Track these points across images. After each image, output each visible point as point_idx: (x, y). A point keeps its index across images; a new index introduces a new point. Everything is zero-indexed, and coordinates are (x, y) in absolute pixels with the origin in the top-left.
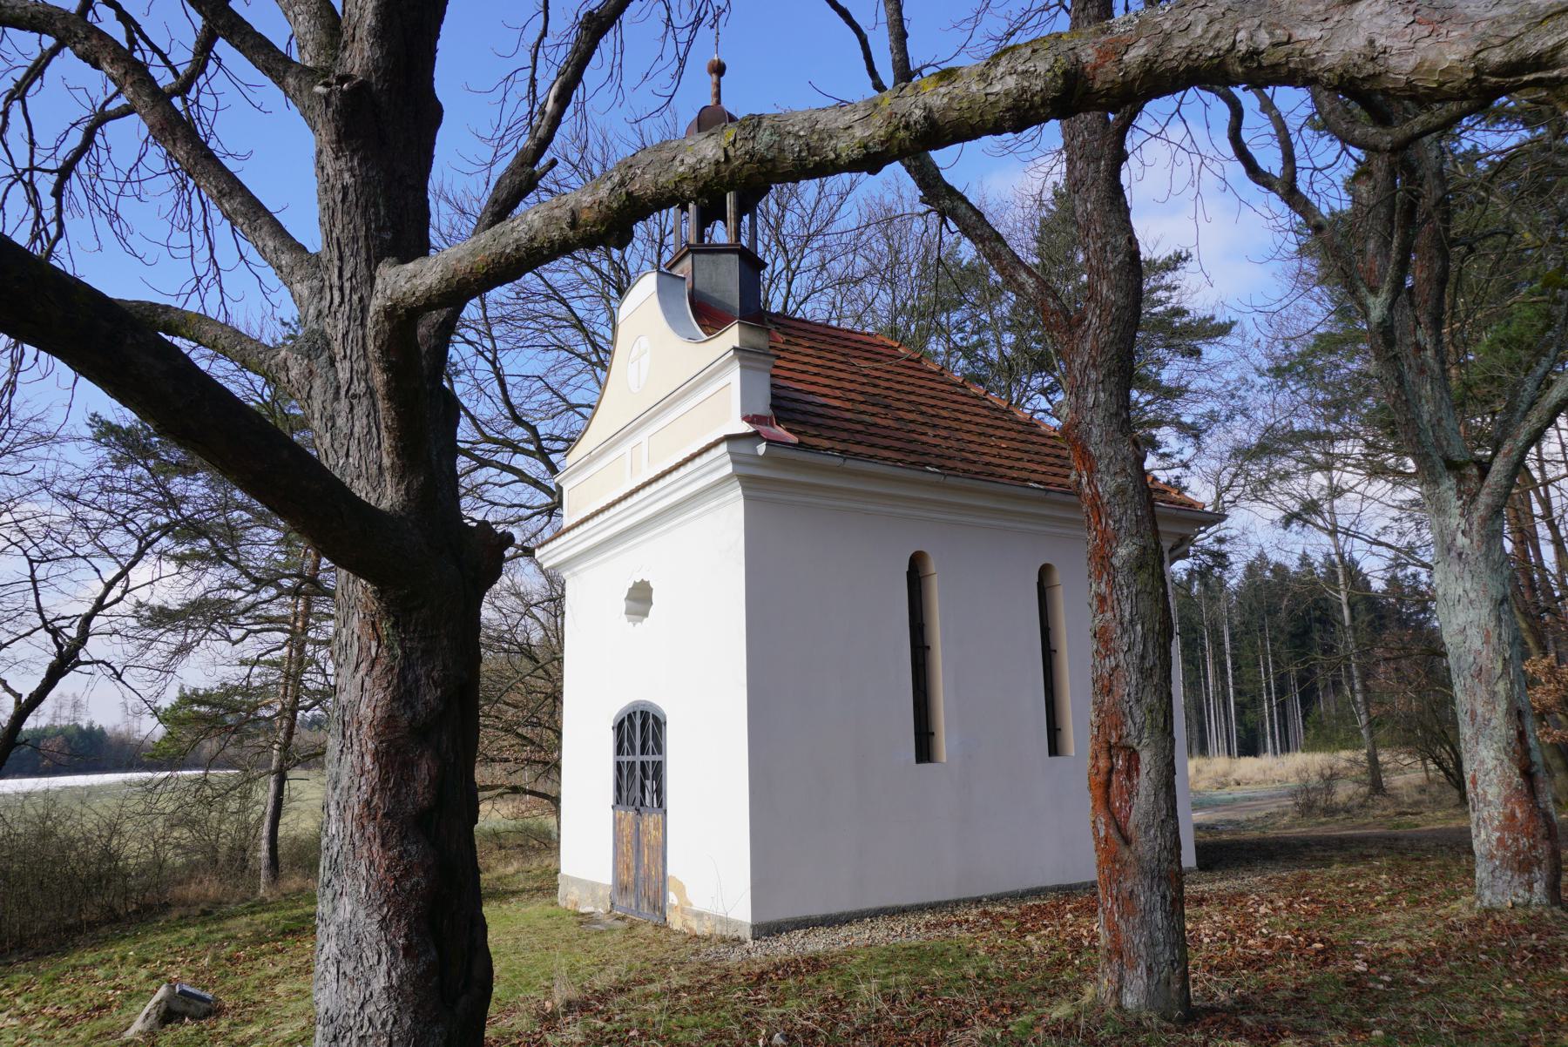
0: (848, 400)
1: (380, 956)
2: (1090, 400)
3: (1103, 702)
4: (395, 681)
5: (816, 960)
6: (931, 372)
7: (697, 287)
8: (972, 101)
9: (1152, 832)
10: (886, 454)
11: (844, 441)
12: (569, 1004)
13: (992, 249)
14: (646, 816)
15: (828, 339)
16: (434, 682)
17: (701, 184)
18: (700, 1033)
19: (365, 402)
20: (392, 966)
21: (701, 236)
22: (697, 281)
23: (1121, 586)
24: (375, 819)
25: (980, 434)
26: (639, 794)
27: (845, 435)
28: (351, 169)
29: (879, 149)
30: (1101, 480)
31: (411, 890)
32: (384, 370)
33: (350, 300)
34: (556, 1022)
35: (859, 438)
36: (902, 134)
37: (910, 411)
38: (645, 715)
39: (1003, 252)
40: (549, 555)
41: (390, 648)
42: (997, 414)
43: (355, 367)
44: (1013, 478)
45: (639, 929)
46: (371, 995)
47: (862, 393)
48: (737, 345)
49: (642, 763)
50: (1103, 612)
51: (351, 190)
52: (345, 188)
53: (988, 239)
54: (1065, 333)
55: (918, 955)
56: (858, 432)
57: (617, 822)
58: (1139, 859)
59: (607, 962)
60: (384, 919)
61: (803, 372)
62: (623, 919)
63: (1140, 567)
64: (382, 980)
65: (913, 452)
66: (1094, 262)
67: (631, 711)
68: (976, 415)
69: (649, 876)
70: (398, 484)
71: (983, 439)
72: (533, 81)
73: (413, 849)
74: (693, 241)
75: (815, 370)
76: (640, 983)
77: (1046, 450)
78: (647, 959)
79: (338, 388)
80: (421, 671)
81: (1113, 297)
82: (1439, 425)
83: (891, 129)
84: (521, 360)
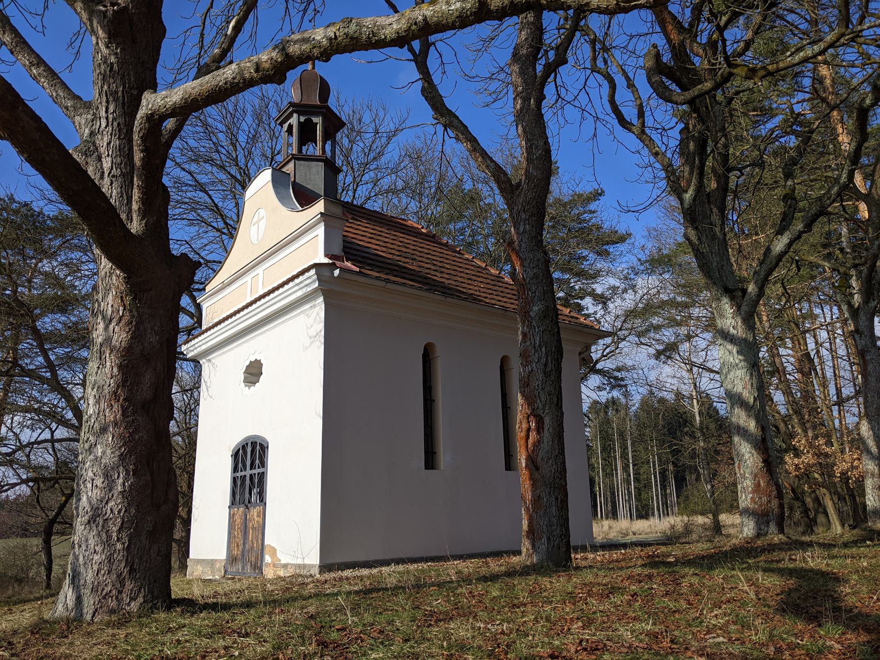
0: (390, 254)
3: (524, 391)
4: (133, 329)
8: (443, 13)
9: (550, 462)
11: (387, 274)
14: (252, 509)
17: (322, 49)
20: (126, 479)
23: (534, 327)
24: (118, 401)
26: (247, 495)
27: (388, 271)
28: (116, 54)
29: (404, 34)
32: (142, 151)
33: (112, 124)
36: (414, 27)
37: (427, 263)
38: (254, 444)
41: (131, 311)
42: (479, 270)
44: (487, 303)
46: (113, 496)
48: (323, 211)
49: (251, 475)
51: (115, 65)
56: (395, 270)
57: (231, 517)
58: (543, 477)
60: (122, 454)
61: (363, 236)
63: (545, 317)
67: (245, 443)
71: (470, 282)
72: (202, 35)
77: (508, 291)
79: (103, 173)
82: (722, 268)
83: (409, 25)
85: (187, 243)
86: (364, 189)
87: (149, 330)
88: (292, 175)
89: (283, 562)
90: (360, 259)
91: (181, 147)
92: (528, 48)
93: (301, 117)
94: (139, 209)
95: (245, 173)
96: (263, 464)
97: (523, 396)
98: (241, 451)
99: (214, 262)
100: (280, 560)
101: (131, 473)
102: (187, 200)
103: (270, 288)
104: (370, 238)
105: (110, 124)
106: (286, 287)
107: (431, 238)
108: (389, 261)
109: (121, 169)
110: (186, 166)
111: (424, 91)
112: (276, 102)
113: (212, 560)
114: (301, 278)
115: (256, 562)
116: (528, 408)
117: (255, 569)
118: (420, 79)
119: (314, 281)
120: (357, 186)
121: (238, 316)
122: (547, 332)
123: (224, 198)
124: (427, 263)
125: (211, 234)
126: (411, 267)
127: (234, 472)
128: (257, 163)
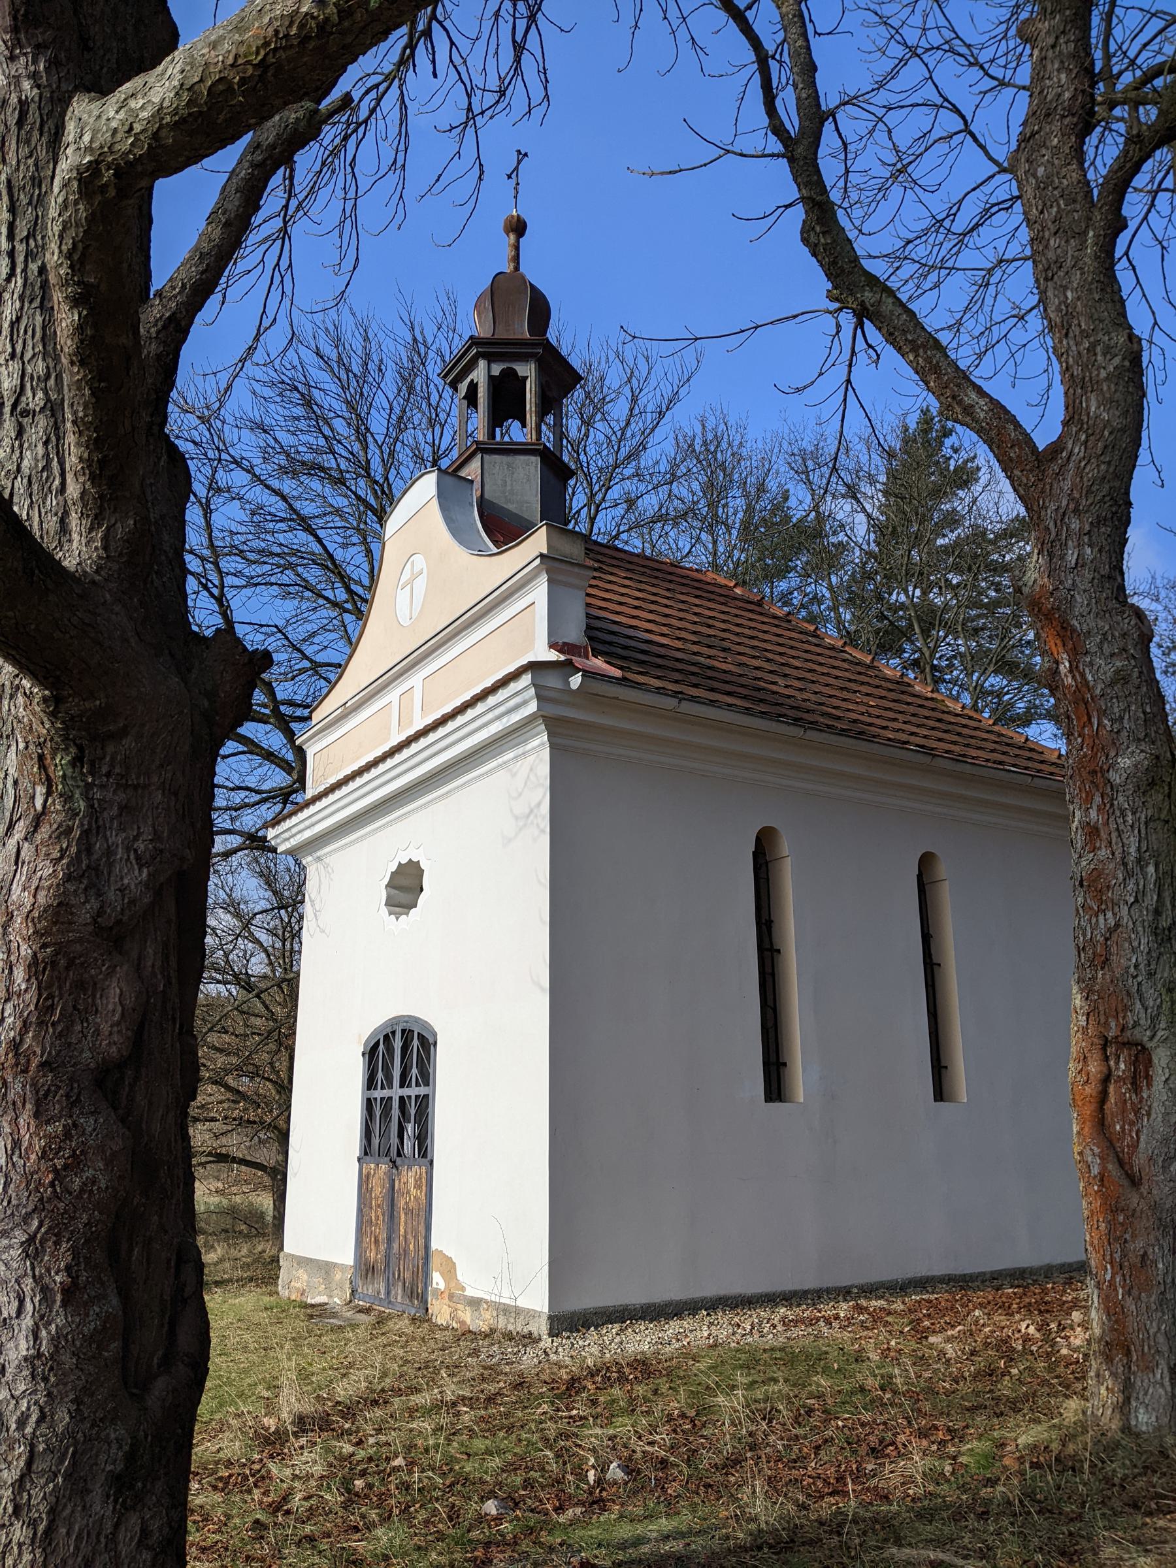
0: (678, 639)
1: (21, 1302)
2: (1071, 557)
3: (1094, 978)
4: (73, 850)
6: (775, 617)
7: (486, 496)
10: (729, 700)
11: (676, 682)
12: (302, 1423)
13: (928, 360)
14: (404, 1170)
15: (648, 571)
16: (138, 858)
18: (496, 1462)
19: (42, 421)
20: (42, 1320)
21: (492, 435)
22: (486, 488)
24: (25, 1071)
25: (842, 688)
26: (395, 1141)
27: (677, 676)
28: (34, 76)
30: (1091, 664)
31: (82, 1191)
32: (75, 302)
34: (282, 1445)
35: (694, 679)
37: (754, 657)
38: (407, 1034)
39: (944, 364)
40: (286, 835)
41: (67, 798)
42: (859, 668)
43: (29, 369)
44: (889, 739)
45: (391, 1324)
47: (694, 633)
48: (545, 552)
49: (402, 1098)
50: (1094, 850)
52: (23, 104)
53: (924, 346)
54: (1031, 471)
55: (787, 1357)
56: (693, 674)
57: (364, 1180)
58: (1154, 1207)
59: (351, 1365)
60: (31, 1239)
61: (621, 603)
62: (367, 1311)
63: (1152, 784)
64: (23, 1345)
65: (761, 701)
66: (1077, 371)
67: (389, 1030)
68: (834, 667)
70: (91, 530)
71: (845, 695)
73: (88, 1123)
74: (481, 436)
75: (636, 603)
76: (399, 1392)
78: (407, 1362)
80: (116, 838)
81: (1105, 416)
84: (253, 604)
85: (280, 631)
86: (610, 517)
89: (470, 1292)
90: (620, 651)
94: (83, 494)
95: (383, 492)
96: (426, 1078)
98: (381, 1047)
100: (463, 1289)
101: (59, 1297)
102: (276, 549)
103: (438, 715)
104: (636, 607)
105: (18, 270)
106: (470, 713)
110: (275, 484)
113: (327, 1263)
114: (502, 694)
117: (411, 1298)
121: (374, 772)
122: (1159, 825)
125: (323, 613)
126: (724, 667)
127: (369, 1089)
128: (406, 474)
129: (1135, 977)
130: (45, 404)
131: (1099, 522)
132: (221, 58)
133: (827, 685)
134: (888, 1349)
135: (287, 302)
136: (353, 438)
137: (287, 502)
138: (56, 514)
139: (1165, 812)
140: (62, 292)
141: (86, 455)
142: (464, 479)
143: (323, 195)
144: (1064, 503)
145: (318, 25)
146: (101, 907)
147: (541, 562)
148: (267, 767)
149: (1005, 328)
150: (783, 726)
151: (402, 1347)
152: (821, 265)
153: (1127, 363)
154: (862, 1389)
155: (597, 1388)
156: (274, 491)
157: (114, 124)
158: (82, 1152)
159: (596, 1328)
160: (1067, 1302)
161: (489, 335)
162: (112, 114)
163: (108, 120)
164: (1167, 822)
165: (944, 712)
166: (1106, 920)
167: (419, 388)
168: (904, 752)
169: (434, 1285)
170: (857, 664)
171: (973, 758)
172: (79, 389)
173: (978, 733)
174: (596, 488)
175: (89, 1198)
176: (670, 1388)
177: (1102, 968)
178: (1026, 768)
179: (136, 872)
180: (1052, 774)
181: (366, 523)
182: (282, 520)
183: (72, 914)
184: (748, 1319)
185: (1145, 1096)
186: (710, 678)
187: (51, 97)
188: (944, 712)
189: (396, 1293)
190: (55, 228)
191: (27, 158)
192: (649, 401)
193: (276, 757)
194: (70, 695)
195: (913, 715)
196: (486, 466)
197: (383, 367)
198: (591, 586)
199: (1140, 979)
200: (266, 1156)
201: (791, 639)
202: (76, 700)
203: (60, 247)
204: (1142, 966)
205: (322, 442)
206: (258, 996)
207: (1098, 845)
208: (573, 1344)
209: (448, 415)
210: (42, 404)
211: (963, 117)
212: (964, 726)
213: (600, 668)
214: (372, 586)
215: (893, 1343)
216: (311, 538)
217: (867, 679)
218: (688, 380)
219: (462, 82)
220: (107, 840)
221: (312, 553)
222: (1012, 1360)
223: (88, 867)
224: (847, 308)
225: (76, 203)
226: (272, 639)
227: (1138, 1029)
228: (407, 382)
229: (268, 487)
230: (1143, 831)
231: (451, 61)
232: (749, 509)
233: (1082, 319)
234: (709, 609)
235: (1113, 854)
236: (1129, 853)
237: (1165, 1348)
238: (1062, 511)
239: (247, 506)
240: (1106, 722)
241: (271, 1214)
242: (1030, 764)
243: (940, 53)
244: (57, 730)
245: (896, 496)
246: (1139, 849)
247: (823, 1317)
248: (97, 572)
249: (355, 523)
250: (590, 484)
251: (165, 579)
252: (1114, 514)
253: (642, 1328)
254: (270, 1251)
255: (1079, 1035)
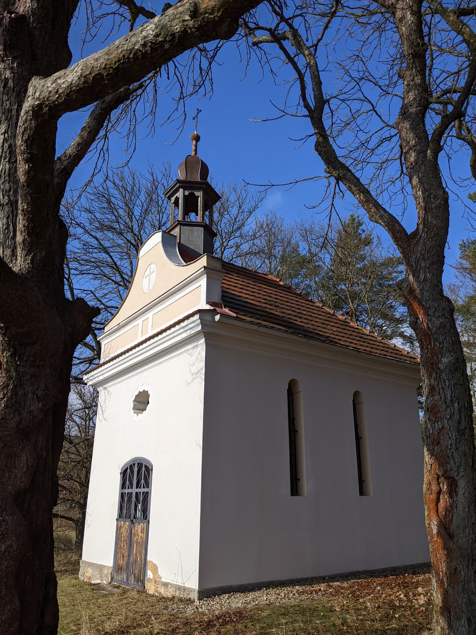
0: (258, 301)
3: (434, 449)
4: (9, 394)
5: (240, 613)
7: (182, 242)
11: (258, 319)
16: (38, 398)
26: (133, 511)
27: (258, 317)
28: (12, 69)
32: (27, 161)
37: (288, 310)
38: (140, 465)
44: (342, 345)
45: (129, 593)
47: (264, 299)
48: (206, 265)
49: (137, 493)
50: (433, 396)
51: (10, 81)
54: (405, 242)
56: (264, 316)
57: (119, 529)
59: (112, 613)
61: (235, 287)
62: (118, 587)
63: (456, 370)
67: (132, 463)
68: (319, 315)
69: (136, 561)
70: (26, 255)
71: (323, 326)
74: (180, 218)
85: (92, 293)
86: (229, 252)
87: (30, 396)
88: (178, 238)
89: (164, 580)
91: (90, 218)
92: (417, 107)
93: (186, 191)
94: (24, 240)
95: (138, 239)
97: (432, 453)
98: (129, 470)
99: (112, 307)
100: (161, 578)
102: (93, 260)
103: (159, 330)
104: (241, 288)
106: (173, 330)
107: (287, 289)
108: (258, 308)
109: (9, 196)
110: (94, 234)
111: (318, 146)
112: (163, 185)
113: (101, 565)
114: (186, 322)
115: (139, 576)
116: (439, 468)
118: (316, 133)
119: (198, 325)
120: (224, 249)
123: (121, 259)
124: (288, 310)
126: (276, 313)
127: (122, 488)
128: (148, 232)
129: (450, 450)
130: (8, 202)
131: (432, 263)
132: (99, 65)
133: (317, 322)
134: (343, 605)
135: (105, 163)
136: (126, 217)
137: (98, 241)
138: (10, 248)
139: (461, 381)
140: (21, 156)
141: (26, 224)
142: (173, 235)
143: (122, 122)
144: (419, 255)
145: (142, 54)
146: (20, 420)
147: (204, 269)
148: (83, 349)
149: (387, 185)
150: (300, 338)
151: (134, 605)
152: (323, 159)
153: (443, 202)
154: (334, 625)
155: (220, 625)
156: (93, 237)
157: (50, 89)
158: (6, 533)
159: (218, 596)
160: (414, 582)
161: (184, 179)
162: (49, 85)
163: (48, 87)
164: (462, 385)
165: (362, 334)
166: (439, 425)
167: (154, 198)
168: (348, 350)
169: (148, 576)
170: (328, 314)
171: (375, 353)
172: (26, 197)
173: (376, 343)
174: (224, 240)
175: (9, 554)
176: (252, 625)
177: (437, 445)
178: (395, 358)
179: (37, 405)
180: (405, 360)
181: (130, 250)
182: (96, 248)
183: (7, 423)
184: (283, 592)
185: (455, 500)
186: (270, 318)
187: (18, 77)
188: (362, 334)
189: (131, 579)
190: (21, 130)
191: (6, 101)
192: (246, 207)
193: (88, 345)
194: (12, 326)
195: (351, 335)
196: (181, 231)
197: (140, 189)
198: (224, 279)
199: (452, 450)
200: (75, 514)
201: (302, 303)
202: (15, 328)
203: (22, 138)
204: (453, 445)
205: (114, 218)
206: (74, 446)
207: (434, 394)
208: (208, 604)
209: (166, 209)
210: (7, 201)
211: (372, 105)
212: (371, 340)
213: (226, 313)
214: (132, 276)
215: (345, 602)
216: (107, 256)
217: (332, 320)
218: (262, 200)
219: (179, 82)
220: (24, 390)
221: (107, 262)
222: (395, 610)
223: (15, 402)
224: (333, 176)
225: (31, 120)
226: (89, 296)
227: (452, 471)
228: (149, 195)
229: (91, 235)
230: (453, 389)
231: (175, 73)
232: (284, 251)
233: (425, 184)
234: (270, 290)
235: (441, 398)
236: (447, 398)
237: (465, 610)
238: (418, 259)
239: (82, 242)
240: (437, 343)
241: (75, 540)
242: (397, 356)
243: (364, 80)
244: (5, 341)
245: (342, 248)
246: (451, 396)
247: (314, 590)
248: (28, 273)
249: (126, 250)
250: (222, 239)
251: (55, 276)
252: (438, 261)
253: (238, 596)
254: (75, 558)
255: (428, 473)
